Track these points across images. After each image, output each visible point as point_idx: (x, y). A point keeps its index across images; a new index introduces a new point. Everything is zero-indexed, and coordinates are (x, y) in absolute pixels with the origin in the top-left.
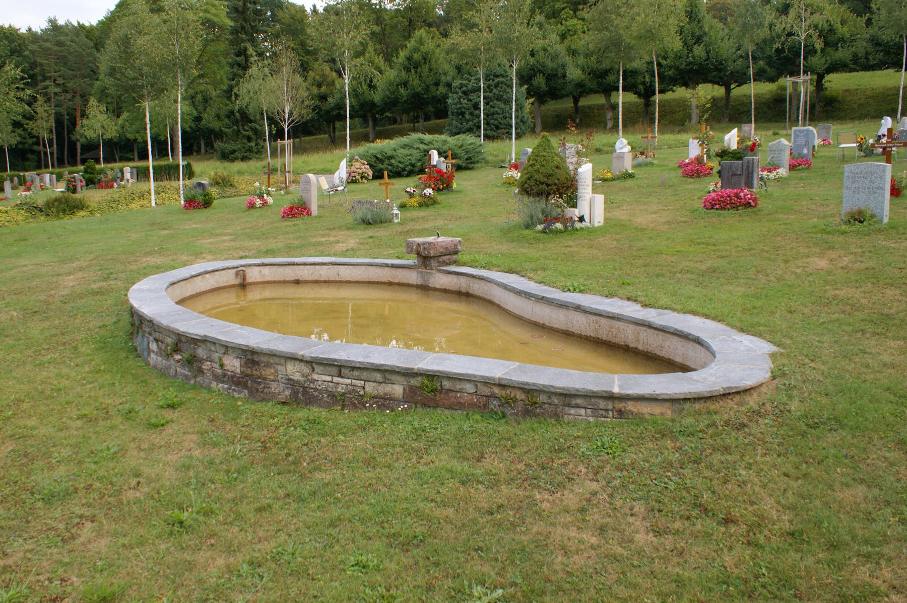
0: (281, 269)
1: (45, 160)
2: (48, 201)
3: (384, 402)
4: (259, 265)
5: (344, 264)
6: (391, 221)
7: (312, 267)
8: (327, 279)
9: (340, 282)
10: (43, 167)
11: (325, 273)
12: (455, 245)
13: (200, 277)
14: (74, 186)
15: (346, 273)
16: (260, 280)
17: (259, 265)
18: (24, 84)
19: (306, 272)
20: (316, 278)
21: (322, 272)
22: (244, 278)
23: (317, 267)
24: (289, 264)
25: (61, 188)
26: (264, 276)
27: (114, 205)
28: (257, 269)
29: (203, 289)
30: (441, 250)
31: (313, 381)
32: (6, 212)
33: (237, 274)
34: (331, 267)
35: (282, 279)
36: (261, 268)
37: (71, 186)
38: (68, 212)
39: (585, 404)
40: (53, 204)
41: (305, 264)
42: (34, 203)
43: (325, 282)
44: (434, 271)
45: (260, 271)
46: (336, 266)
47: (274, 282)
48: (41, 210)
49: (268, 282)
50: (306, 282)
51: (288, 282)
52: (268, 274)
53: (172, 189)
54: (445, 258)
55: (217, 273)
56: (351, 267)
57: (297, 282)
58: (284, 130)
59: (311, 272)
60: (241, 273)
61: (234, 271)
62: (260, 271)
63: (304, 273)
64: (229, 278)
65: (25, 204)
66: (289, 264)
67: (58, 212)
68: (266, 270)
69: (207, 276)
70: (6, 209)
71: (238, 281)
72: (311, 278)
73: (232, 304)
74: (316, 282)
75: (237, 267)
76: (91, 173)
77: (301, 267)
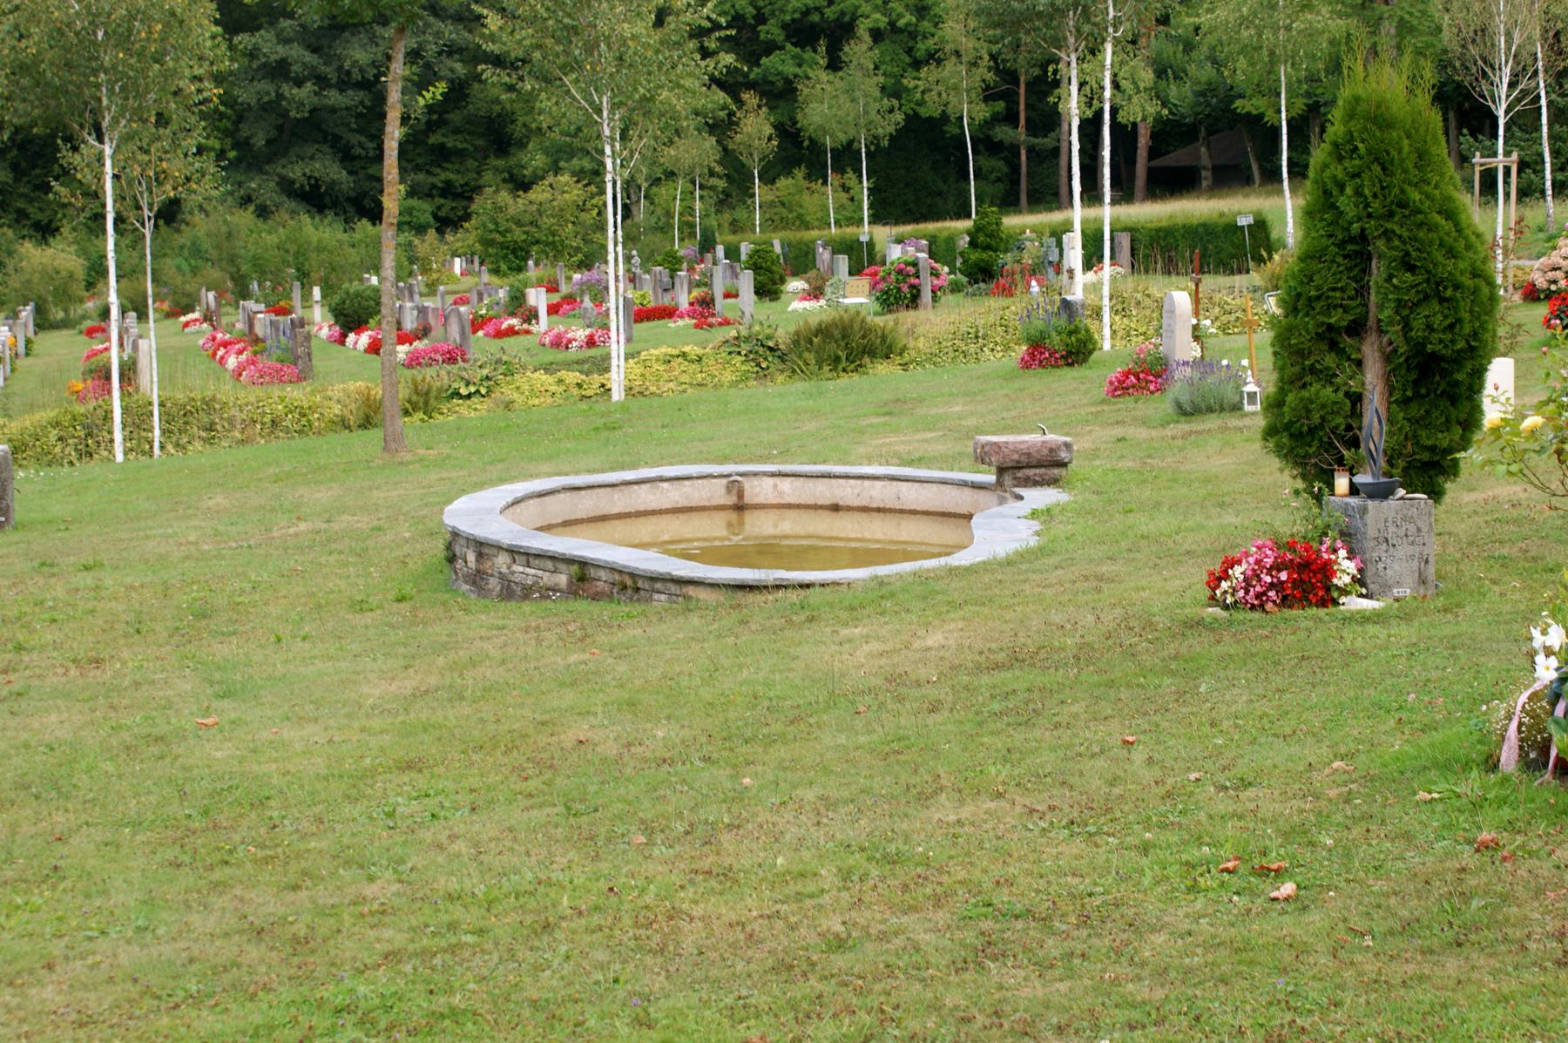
0: (811, 483)
1: (1131, 161)
2: (797, 333)
3: (547, 592)
4: (773, 475)
5: (847, 477)
6: (1237, 408)
7: (859, 482)
8: (881, 506)
9: (902, 511)
10: (1023, 198)
11: (878, 493)
12: (1051, 450)
13: (648, 485)
14: (912, 287)
15: (911, 496)
16: (775, 502)
17: (773, 475)
18: (719, 39)
19: (849, 490)
20: (864, 503)
21: (874, 493)
22: (740, 495)
23: (867, 483)
24: (823, 476)
25: (857, 294)
26: (781, 493)
27: (973, 348)
28: (770, 481)
29: (654, 506)
30: (1016, 457)
31: (513, 573)
32: (700, 359)
33: (729, 490)
34: (887, 483)
35: (811, 502)
36: (777, 480)
37: (905, 289)
38: (843, 364)
39: (662, 589)
40: (811, 342)
41: (847, 477)
42: (769, 338)
43: (879, 510)
44: (1008, 495)
45: (775, 486)
46: (894, 483)
47: (799, 507)
48: (782, 358)
49: (789, 506)
50: (849, 509)
51: (821, 507)
52: (789, 490)
53: (1147, 302)
54: (1031, 472)
55: (687, 483)
56: (917, 484)
57: (835, 508)
58: (1495, 119)
59: (856, 491)
60: (735, 487)
61: (724, 481)
62: (775, 486)
63: (846, 492)
64: (715, 492)
65: (747, 339)
66: (823, 476)
67: (820, 364)
68: (786, 485)
69: (665, 485)
70: (699, 351)
71: (731, 500)
72: (856, 503)
73: (715, 539)
74: (865, 509)
75: (729, 475)
76: (987, 247)
77: (841, 481)
